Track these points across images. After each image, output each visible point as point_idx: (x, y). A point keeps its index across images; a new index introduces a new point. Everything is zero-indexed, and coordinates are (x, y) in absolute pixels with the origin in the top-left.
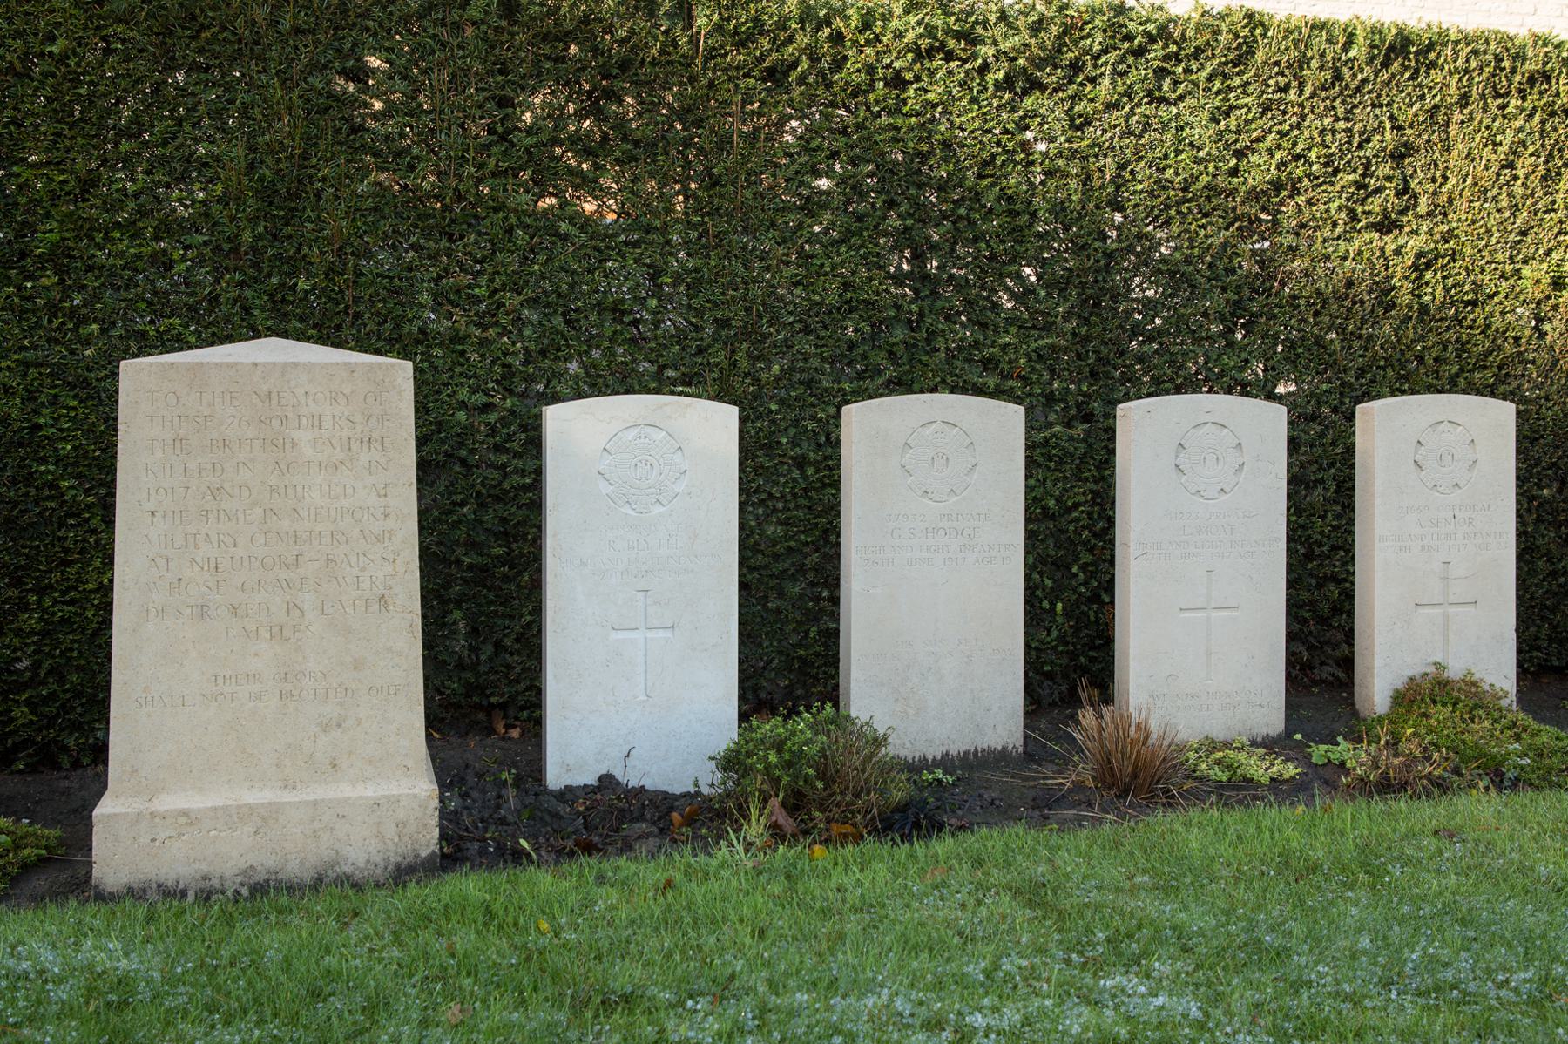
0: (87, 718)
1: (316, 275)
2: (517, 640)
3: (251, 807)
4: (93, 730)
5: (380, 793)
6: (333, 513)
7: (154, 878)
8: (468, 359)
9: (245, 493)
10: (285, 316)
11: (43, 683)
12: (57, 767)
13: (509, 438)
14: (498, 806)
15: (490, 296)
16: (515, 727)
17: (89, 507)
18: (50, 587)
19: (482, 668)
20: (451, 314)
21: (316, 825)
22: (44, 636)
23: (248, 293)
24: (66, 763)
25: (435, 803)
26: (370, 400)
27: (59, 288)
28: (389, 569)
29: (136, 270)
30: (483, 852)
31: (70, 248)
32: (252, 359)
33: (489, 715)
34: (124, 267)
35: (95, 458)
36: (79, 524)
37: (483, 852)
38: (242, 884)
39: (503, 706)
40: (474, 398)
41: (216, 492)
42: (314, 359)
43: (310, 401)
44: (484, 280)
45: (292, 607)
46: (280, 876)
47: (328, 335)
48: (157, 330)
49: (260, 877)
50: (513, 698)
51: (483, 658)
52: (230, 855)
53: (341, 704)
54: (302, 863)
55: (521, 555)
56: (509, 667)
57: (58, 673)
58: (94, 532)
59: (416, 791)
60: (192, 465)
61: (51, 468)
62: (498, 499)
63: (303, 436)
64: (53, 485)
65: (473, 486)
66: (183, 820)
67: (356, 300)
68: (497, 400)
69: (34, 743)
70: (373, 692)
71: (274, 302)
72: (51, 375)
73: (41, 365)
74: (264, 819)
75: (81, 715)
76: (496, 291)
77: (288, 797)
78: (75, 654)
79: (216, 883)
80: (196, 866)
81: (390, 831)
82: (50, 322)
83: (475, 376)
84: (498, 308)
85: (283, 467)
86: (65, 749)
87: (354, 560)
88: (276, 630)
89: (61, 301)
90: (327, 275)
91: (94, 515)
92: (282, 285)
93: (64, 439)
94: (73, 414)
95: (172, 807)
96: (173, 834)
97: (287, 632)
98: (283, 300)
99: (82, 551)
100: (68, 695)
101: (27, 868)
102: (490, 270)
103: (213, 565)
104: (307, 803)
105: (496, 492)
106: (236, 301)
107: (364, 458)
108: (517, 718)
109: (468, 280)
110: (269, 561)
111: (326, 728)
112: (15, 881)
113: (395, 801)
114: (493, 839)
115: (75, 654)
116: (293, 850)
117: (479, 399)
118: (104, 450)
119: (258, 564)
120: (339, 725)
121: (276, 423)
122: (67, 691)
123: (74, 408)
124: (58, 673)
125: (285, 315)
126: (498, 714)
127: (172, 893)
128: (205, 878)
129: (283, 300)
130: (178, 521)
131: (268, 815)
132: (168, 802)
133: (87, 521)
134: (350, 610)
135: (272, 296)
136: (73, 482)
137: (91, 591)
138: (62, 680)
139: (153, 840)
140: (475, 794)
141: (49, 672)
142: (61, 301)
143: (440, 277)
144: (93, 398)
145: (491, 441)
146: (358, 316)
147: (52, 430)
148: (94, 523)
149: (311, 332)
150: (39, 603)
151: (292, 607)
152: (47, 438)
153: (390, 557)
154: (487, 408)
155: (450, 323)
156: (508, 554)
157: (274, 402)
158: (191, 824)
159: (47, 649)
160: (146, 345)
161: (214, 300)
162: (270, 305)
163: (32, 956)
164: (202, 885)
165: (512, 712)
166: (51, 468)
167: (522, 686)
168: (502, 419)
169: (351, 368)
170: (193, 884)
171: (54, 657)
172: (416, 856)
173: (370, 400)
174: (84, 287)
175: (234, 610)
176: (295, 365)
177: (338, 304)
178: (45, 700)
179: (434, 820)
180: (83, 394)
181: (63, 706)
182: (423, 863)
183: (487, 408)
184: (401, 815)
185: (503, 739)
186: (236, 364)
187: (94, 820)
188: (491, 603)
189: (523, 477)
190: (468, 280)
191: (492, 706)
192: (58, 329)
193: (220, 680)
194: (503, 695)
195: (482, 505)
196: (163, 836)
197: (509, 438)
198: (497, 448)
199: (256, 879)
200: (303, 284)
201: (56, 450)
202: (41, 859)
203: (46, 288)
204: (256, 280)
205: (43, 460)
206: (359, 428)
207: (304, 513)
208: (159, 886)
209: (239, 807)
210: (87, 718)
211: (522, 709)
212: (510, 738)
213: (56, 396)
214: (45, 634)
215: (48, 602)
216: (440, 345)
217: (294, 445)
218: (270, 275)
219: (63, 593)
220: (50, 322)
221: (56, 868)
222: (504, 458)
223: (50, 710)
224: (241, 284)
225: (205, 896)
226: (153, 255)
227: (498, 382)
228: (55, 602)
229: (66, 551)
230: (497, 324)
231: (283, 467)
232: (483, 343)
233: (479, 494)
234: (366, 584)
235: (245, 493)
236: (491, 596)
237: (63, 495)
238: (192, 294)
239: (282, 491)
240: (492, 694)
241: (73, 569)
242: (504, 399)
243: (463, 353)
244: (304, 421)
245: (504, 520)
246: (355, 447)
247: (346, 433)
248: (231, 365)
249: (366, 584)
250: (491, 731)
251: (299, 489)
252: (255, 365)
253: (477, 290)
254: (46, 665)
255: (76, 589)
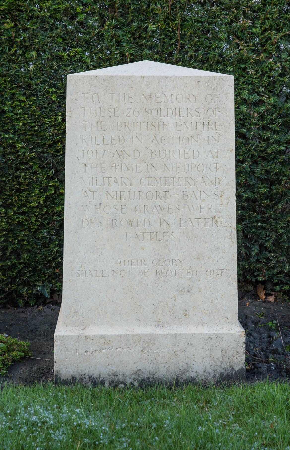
0: (32, 279)
1: (158, 22)
2: (274, 244)
3: (139, 335)
4: (35, 286)
5: (212, 332)
6: (186, 167)
7: (87, 373)
8: (248, 73)
9: (137, 154)
10: (141, 47)
11: (9, 258)
12: (16, 305)
13: (272, 122)
14: (270, 343)
15: (263, 33)
16: (271, 295)
17: (32, 159)
18: (12, 204)
19: (253, 260)
20: (238, 45)
21: (176, 348)
22: (9, 232)
23: (120, 33)
24: (21, 303)
25: (243, 339)
26: (209, 99)
27: (14, 30)
28: (219, 201)
29: (56, 19)
30: (269, 370)
31: (19, 6)
32: (140, 74)
33: (255, 287)
34: (50, 17)
35: (35, 131)
36: (27, 169)
37: (269, 370)
38: (135, 379)
39: (264, 283)
40: (251, 97)
41: (120, 153)
42: (176, 74)
43: (174, 99)
44: (258, 23)
45: (163, 221)
46: (156, 376)
47: (166, 57)
48: (69, 55)
49: (145, 376)
50: (271, 278)
51: (253, 253)
52: (128, 363)
53: (190, 279)
54: (168, 370)
55: (278, 193)
56: (268, 259)
57: (17, 253)
58: (35, 173)
59: (232, 332)
60: (107, 137)
61: (12, 136)
62: (264, 159)
63: (170, 120)
64: (13, 146)
65: (250, 151)
66: (103, 341)
67: (182, 37)
68: (264, 98)
69: (4, 291)
70: (208, 273)
71: (134, 38)
72: (11, 81)
73: (5, 76)
74: (147, 343)
75: (29, 277)
76: (265, 30)
77: (160, 331)
78: (25, 243)
79: (120, 378)
80: (110, 367)
81: (218, 354)
82: (10, 50)
83: (252, 84)
84: (266, 41)
85: (159, 139)
86: (20, 296)
87: (198, 195)
88: (154, 235)
89: (16, 37)
90: (165, 21)
91: (35, 164)
92: (139, 27)
93: (18, 119)
94: (23, 105)
95: (96, 333)
96: (97, 348)
97: (160, 236)
98: (140, 37)
99: (29, 184)
100: (22, 266)
101: (16, 362)
102: (263, 16)
103: (118, 196)
104: (171, 335)
105: (263, 154)
106: (113, 37)
107: (205, 134)
108: (272, 290)
109: (249, 23)
110: (150, 194)
111: (181, 293)
112: (10, 369)
113: (220, 337)
114: (274, 362)
115: (25, 243)
116: (163, 362)
117: (255, 98)
118: (40, 126)
119: (144, 196)
120: (189, 292)
121: (154, 112)
122: (22, 263)
123: (24, 101)
124: (17, 253)
125: (141, 46)
126: (260, 288)
127: (97, 382)
128: (115, 375)
129: (140, 37)
130: (99, 169)
131: (149, 341)
132: (95, 331)
133: (31, 167)
134: (195, 224)
135: (133, 34)
136: (23, 144)
137: (34, 207)
138: (18, 257)
139: (87, 352)
140: (255, 334)
141: (12, 253)
142: (16, 37)
143: (232, 22)
144: (34, 96)
145: (261, 124)
146: (182, 47)
147: (11, 114)
148: (35, 168)
149: (156, 56)
150: (6, 213)
151: (163, 221)
152: (9, 118)
153: (219, 194)
154: (257, 104)
155: (237, 51)
156: (269, 192)
157: (153, 100)
158: (107, 343)
159: (11, 239)
160: (82, 66)
161: (100, 36)
162: (132, 40)
163: (36, 413)
164: (113, 378)
165: (269, 286)
166: (12, 136)
167: (275, 271)
168: (268, 110)
169: (198, 80)
170: (108, 378)
171: (14, 244)
172: (233, 370)
173: (209, 99)
174: (27, 29)
175: (130, 222)
176: (166, 77)
177: (171, 39)
178: (10, 268)
179: (242, 350)
180: (28, 93)
181: (19, 271)
182: (236, 374)
183: (257, 104)
184: (224, 345)
185: (264, 302)
186: (132, 77)
187: (55, 338)
188: (258, 221)
189: (280, 145)
190: (249, 23)
191: (257, 282)
192: (14, 54)
193: (122, 262)
194: (265, 276)
195: (255, 162)
196: (92, 349)
197: (272, 122)
198: (264, 128)
199: (142, 377)
200: (151, 27)
201: (14, 125)
202: (22, 358)
203: (7, 30)
204: (123, 25)
205: (7, 132)
206: (202, 116)
207: (169, 166)
208: (90, 377)
209: (133, 335)
210: (32, 279)
211: (276, 284)
212: (269, 302)
213: (13, 94)
214: (10, 231)
215: (11, 213)
216: (231, 64)
217: (164, 126)
218: (132, 21)
219: (19, 208)
220: (10, 50)
221: (32, 361)
222: (268, 134)
223: (13, 274)
224: (116, 27)
225: (115, 384)
226: (66, 9)
227: (266, 87)
228: (15, 213)
229: (20, 184)
230: (265, 51)
231: (159, 139)
232: (258, 63)
233: (253, 155)
234: (205, 210)
235: (137, 154)
236: (259, 217)
237: (18, 152)
238: (89, 33)
239: (158, 153)
240: (258, 275)
241: (24, 195)
242: (269, 98)
243: (244, 69)
244: (170, 111)
245: (267, 172)
246: (200, 127)
247: (194, 119)
248: (129, 78)
249: (205, 210)
250: (256, 297)
251: (167, 152)
252: (143, 77)
253: (254, 30)
254: (10, 249)
255: (25, 206)
